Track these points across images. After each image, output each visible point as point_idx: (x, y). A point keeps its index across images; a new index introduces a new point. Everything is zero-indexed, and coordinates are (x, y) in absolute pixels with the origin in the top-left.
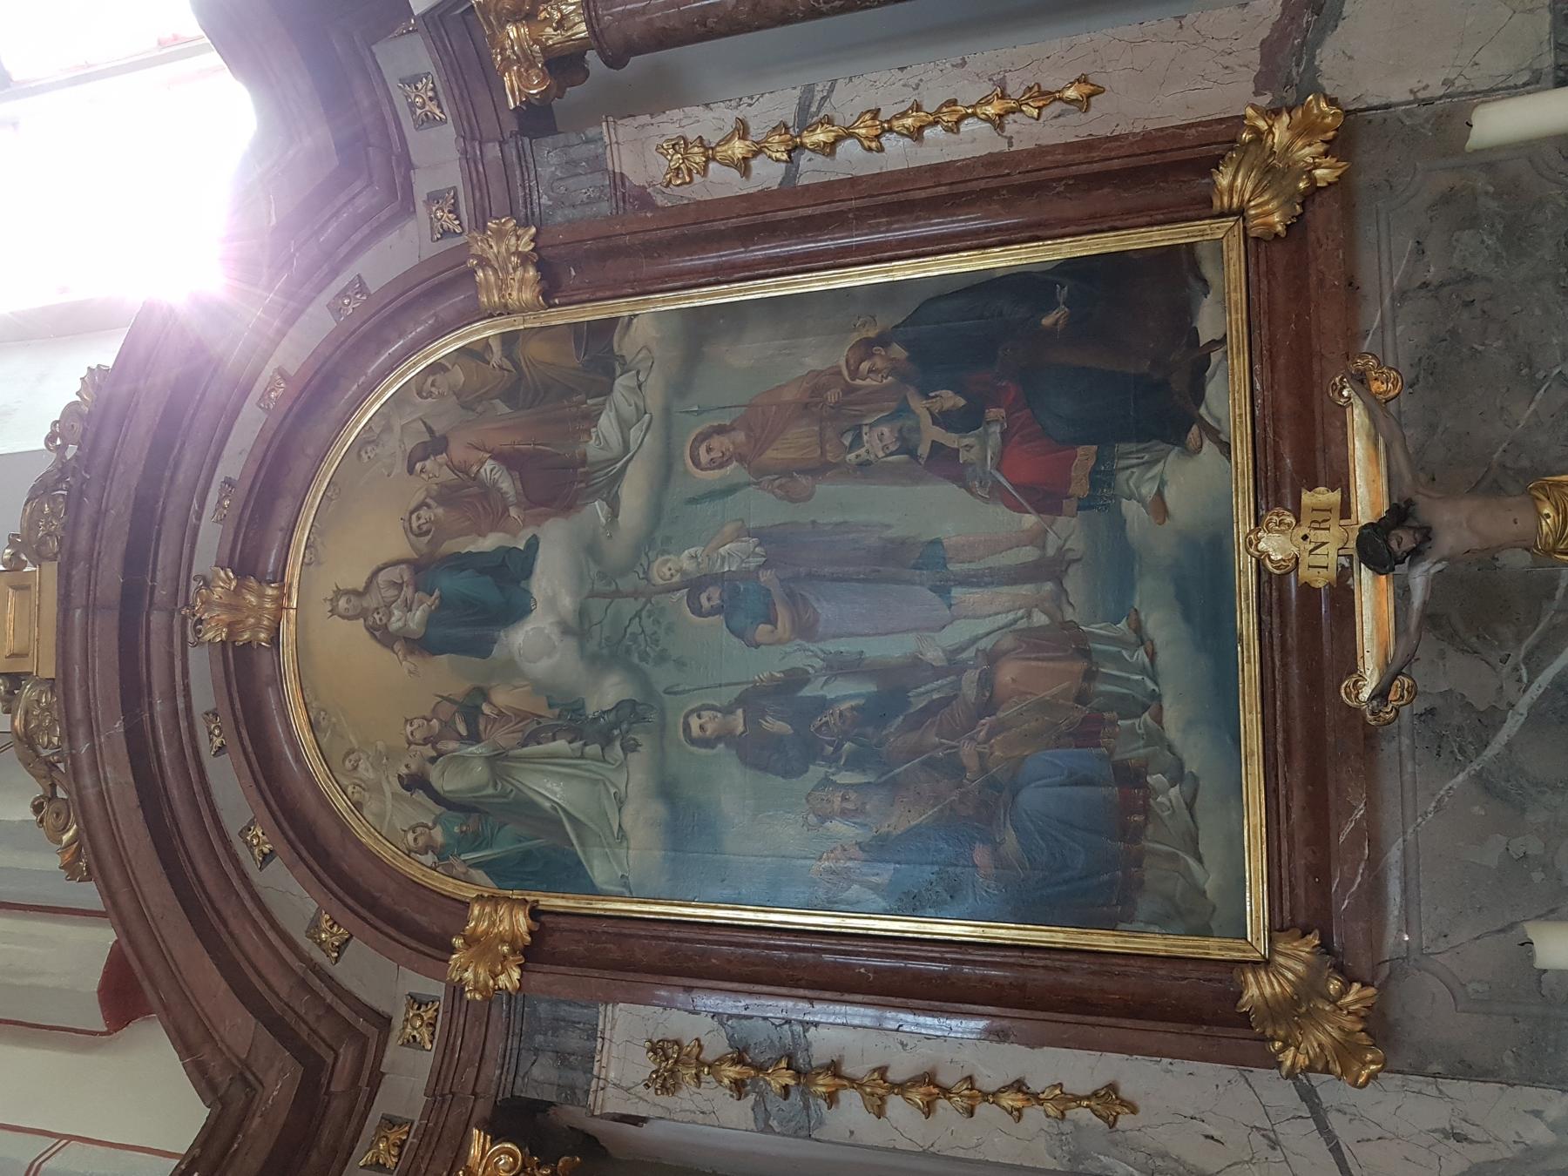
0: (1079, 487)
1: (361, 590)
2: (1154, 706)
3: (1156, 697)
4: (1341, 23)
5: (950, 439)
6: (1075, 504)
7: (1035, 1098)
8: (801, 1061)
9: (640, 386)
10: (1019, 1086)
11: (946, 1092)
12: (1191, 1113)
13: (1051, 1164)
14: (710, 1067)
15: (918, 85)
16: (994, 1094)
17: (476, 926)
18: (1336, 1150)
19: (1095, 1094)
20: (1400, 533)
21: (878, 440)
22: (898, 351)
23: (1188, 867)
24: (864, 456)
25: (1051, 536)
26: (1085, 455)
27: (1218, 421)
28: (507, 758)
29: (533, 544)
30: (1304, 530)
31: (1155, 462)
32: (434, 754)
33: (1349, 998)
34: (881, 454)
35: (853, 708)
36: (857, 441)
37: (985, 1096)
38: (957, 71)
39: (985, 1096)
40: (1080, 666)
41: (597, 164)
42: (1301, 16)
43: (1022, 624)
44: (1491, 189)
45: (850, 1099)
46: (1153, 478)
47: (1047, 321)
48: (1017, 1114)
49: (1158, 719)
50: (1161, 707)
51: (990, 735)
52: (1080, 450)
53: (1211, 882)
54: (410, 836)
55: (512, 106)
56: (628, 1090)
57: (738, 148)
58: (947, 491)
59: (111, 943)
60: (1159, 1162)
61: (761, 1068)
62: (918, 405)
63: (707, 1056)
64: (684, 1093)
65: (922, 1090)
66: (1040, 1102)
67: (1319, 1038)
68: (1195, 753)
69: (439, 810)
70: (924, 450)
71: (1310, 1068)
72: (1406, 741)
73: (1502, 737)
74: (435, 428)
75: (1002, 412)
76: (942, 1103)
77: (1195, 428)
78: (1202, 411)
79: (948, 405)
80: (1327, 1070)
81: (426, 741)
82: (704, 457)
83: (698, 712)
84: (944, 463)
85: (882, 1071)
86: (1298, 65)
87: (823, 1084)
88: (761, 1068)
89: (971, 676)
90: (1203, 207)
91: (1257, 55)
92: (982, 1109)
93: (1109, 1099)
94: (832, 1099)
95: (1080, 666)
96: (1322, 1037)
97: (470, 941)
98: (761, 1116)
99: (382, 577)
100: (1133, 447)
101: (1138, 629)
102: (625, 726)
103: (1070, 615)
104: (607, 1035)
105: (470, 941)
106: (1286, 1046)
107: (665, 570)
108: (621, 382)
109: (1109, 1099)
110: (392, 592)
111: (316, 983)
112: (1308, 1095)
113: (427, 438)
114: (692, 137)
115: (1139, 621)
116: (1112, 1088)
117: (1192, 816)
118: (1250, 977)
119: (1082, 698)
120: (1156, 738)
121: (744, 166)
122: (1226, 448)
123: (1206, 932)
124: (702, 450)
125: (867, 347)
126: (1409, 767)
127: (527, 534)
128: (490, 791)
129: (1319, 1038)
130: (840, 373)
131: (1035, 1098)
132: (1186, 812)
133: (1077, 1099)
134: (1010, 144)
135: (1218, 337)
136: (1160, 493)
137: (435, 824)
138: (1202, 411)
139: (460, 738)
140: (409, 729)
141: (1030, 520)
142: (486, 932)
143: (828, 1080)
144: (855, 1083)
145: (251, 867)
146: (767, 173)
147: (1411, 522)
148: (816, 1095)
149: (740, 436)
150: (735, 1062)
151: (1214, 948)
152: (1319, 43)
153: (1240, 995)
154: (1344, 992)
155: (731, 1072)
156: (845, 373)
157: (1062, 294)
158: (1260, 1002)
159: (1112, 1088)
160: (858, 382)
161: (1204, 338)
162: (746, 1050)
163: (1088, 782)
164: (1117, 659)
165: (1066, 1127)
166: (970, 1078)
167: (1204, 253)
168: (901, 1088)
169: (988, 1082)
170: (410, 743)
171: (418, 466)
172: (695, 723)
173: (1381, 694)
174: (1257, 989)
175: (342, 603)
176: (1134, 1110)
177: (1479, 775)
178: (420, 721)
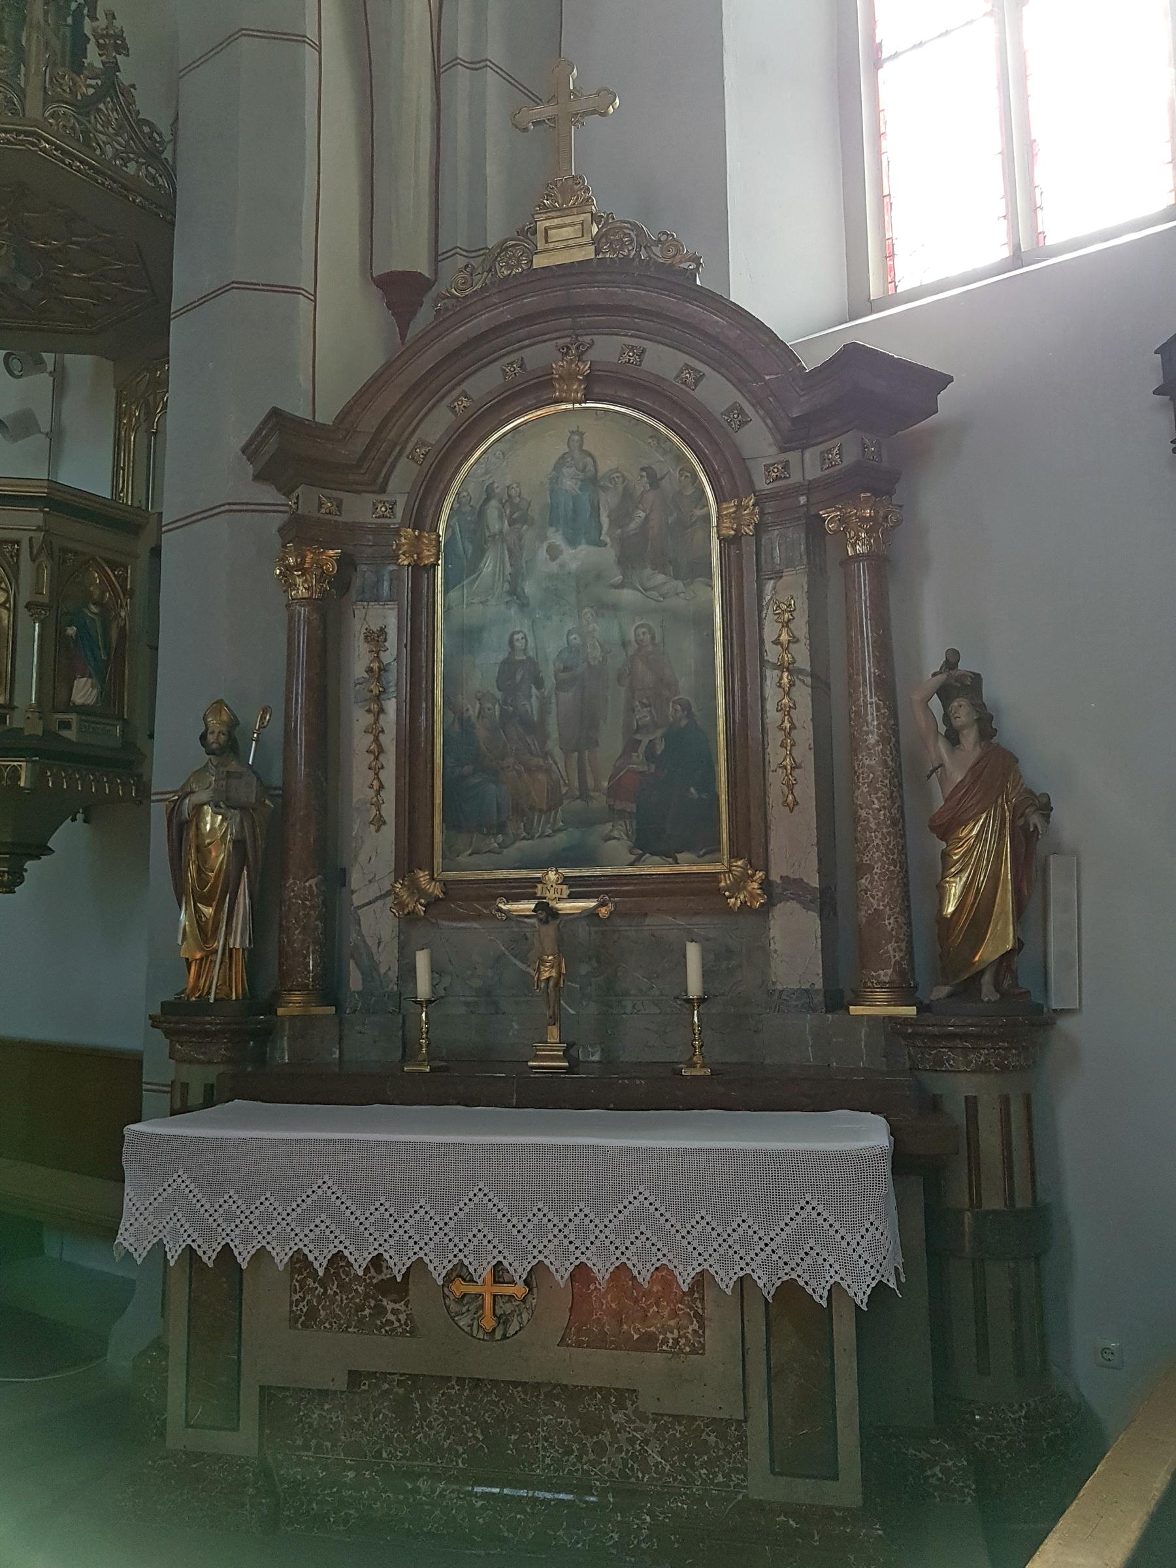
0: (619, 806)
1: (584, 448)
2: (527, 837)
3: (532, 838)
4: (805, 910)
5: (642, 748)
6: (612, 803)
7: (378, 793)
8: (382, 696)
9: (677, 594)
10: (381, 787)
11: (377, 758)
12: (379, 852)
13: (354, 800)
14: (377, 657)
15: (804, 727)
16: (378, 777)
17: (425, 537)
18: (370, 903)
19: (381, 816)
20: (544, 914)
21: (643, 715)
22: (683, 723)
23: (467, 851)
24: (636, 710)
25: (598, 794)
26: (632, 807)
27: (644, 861)
28: (503, 542)
29: (601, 544)
30: (554, 886)
31: (627, 835)
32: (504, 501)
33: (419, 906)
34: (637, 717)
35: (527, 711)
36: (644, 705)
37: (377, 774)
38: (808, 746)
39: (377, 774)
40: (545, 808)
41: (789, 563)
42: (810, 895)
43: (562, 782)
44: (730, 966)
45: (370, 718)
46: (621, 835)
47: (692, 790)
48: (371, 787)
49: (524, 839)
50: (528, 839)
51: (516, 770)
52: (634, 805)
53: (463, 859)
54: (465, 494)
55: (821, 513)
56: (365, 619)
57: (784, 637)
58: (618, 747)
59: (419, 271)
60: (360, 841)
61: (379, 680)
62: (659, 733)
63: (382, 654)
64: (366, 645)
65: (376, 749)
66: (376, 796)
67: (404, 895)
68: (512, 852)
69: (478, 507)
70: (638, 737)
71: (396, 893)
72: (516, 930)
73: (518, 963)
74: (663, 481)
75: (653, 771)
76: (372, 757)
77: (641, 852)
78: (648, 855)
79: (658, 747)
80: (395, 899)
81: (509, 496)
82: (641, 631)
83: (525, 638)
84: (632, 745)
85: (383, 731)
86: (791, 894)
87: (374, 707)
88: (379, 680)
89: (541, 762)
90: (734, 856)
91: (797, 877)
92: (372, 773)
93: (380, 822)
94: (369, 711)
95: (545, 808)
96: (405, 897)
97: (418, 538)
98: (360, 681)
99: (589, 459)
100: (634, 827)
101: (560, 830)
102: (518, 601)
103: (566, 802)
104: (387, 606)
105: (418, 538)
106: (401, 884)
107: (589, 615)
108: (680, 584)
109: (380, 822)
110: (581, 466)
111: (397, 450)
112: (388, 894)
113: (658, 477)
114: (795, 614)
115: (562, 830)
116: (384, 823)
117: (486, 852)
118: (427, 873)
119: (532, 808)
120: (517, 838)
121: (777, 642)
122: (632, 864)
123: (443, 858)
124: (644, 630)
125: (687, 707)
126: (507, 930)
127: (608, 540)
128: (487, 534)
129: (404, 895)
130: (675, 695)
131: (378, 793)
132: (487, 850)
133: (379, 810)
134: (773, 771)
135: (679, 861)
136: (615, 838)
137: (471, 506)
138: (648, 855)
139: (512, 514)
140: (515, 486)
141: (605, 784)
142: (423, 543)
143: (376, 710)
144: (377, 721)
145: (448, 400)
146: (772, 653)
147: (550, 918)
148: (370, 704)
149: (650, 648)
150: (379, 668)
151: (438, 860)
152: (800, 902)
153: (420, 869)
154: (421, 904)
155: (375, 666)
156: (676, 698)
157: (704, 796)
158: (417, 877)
159: (384, 823)
160: (671, 704)
161: (678, 856)
162: (386, 671)
163: (499, 811)
164: (547, 822)
165: (369, 805)
166: (383, 767)
167: (716, 856)
168: (376, 739)
169: (382, 774)
170: (508, 487)
171: (644, 474)
172: (519, 636)
173: (500, 910)
174: (423, 876)
175: (576, 438)
176: (377, 831)
177: (504, 954)
178: (518, 491)
